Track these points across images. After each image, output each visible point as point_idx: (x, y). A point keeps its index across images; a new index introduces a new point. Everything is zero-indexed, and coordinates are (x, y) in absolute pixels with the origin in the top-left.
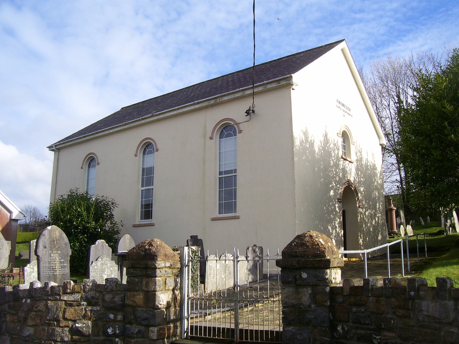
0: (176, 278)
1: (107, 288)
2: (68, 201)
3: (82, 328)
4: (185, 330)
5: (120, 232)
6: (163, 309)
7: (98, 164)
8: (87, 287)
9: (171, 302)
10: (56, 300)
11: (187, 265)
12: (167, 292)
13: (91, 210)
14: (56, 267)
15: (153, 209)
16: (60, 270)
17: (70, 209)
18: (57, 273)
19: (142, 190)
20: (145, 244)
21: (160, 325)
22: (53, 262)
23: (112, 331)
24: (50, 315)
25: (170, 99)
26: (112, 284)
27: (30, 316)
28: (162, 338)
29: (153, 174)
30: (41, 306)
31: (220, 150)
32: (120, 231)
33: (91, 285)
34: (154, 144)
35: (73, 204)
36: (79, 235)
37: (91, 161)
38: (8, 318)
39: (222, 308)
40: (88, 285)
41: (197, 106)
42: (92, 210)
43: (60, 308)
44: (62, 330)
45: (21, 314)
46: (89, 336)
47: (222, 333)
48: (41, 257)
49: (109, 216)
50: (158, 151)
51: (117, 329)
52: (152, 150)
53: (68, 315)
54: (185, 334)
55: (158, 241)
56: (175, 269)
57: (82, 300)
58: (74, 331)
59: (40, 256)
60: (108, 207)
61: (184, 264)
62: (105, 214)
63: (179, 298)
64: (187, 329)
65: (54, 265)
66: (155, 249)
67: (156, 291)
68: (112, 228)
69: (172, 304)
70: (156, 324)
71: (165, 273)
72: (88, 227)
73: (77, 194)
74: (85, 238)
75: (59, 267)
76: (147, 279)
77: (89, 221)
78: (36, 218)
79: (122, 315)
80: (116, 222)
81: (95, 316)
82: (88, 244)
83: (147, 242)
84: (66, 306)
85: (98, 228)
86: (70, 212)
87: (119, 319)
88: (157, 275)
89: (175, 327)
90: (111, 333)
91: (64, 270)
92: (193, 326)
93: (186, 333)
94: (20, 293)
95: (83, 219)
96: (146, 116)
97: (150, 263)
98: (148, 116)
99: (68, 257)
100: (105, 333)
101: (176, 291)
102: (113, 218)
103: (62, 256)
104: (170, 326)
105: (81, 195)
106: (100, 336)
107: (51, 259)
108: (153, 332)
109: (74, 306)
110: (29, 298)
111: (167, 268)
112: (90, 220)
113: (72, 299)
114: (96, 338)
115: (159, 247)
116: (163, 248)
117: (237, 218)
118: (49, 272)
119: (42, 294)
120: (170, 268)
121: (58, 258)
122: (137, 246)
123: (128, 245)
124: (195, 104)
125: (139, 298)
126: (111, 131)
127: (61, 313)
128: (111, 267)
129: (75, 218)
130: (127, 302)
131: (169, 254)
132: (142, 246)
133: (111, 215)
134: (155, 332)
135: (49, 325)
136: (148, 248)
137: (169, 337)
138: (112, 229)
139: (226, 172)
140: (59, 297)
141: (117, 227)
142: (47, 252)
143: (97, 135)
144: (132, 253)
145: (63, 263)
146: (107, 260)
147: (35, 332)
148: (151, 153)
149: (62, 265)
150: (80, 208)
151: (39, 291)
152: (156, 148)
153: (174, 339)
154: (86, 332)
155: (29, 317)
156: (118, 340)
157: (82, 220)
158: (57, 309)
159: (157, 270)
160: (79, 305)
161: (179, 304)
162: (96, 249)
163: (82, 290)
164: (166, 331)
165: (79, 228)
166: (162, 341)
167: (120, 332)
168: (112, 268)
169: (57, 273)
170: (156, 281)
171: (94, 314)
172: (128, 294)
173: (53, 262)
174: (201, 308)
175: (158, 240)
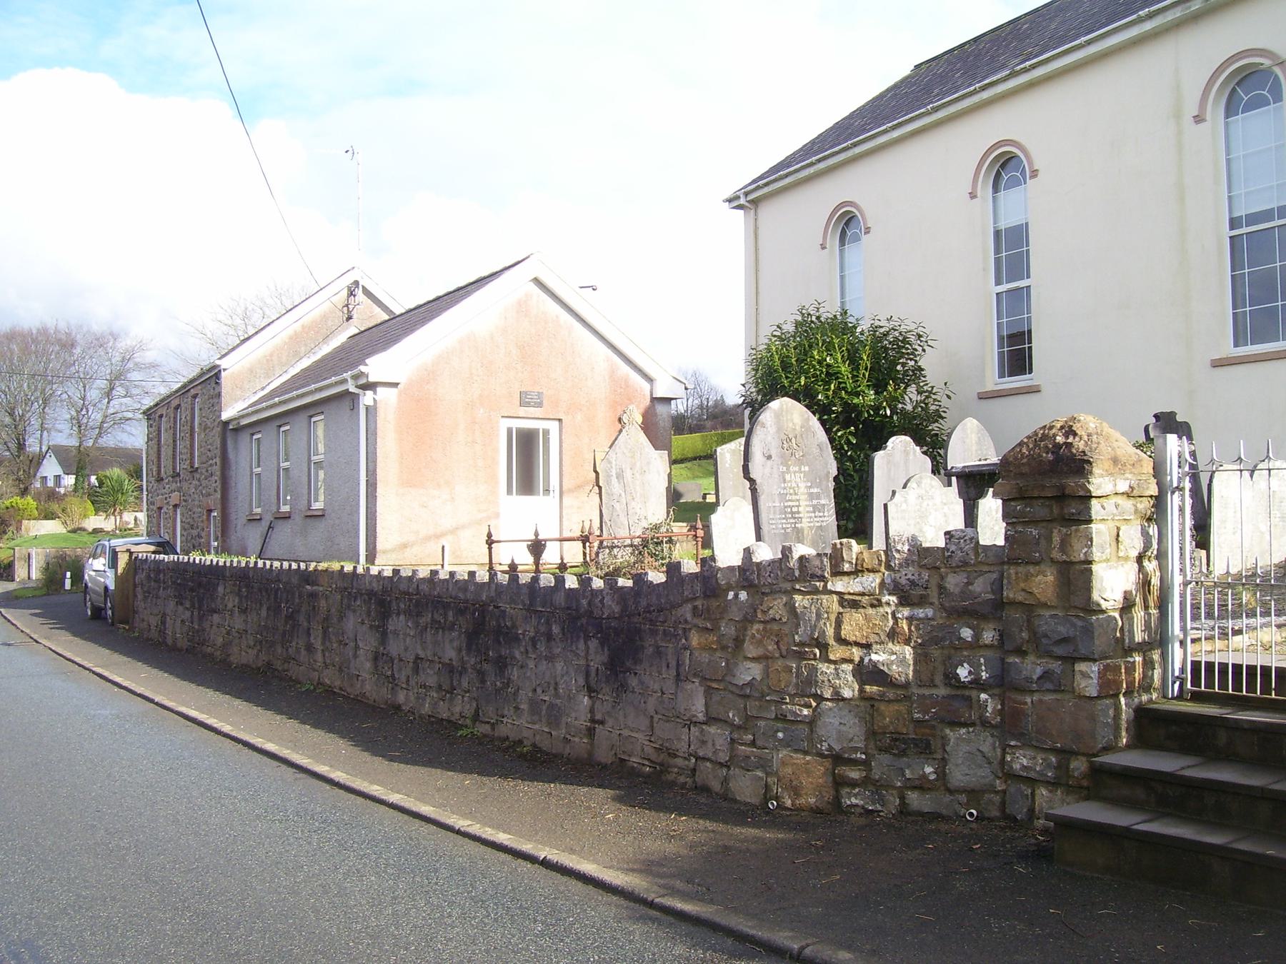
0: (1146, 524)
1: (950, 556)
2: (798, 339)
3: (887, 665)
4: (1177, 673)
5: (943, 414)
6: (1112, 614)
7: (868, 230)
8: (897, 556)
9: (1134, 592)
10: (816, 591)
11: (1177, 488)
12: (1122, 565)
13: (862, 359)
14: (801, 509)
15: (1033, 345)
16: (811, 517)
17: (804, 360)
18: (803, 525)
19: (997, 294)
20: (1054, 431)
21: (1106, 658)
22: (791, 494)
23: (970, 672)
24: (801, 631)
25: (1058, 20)
26: (963, 545)
27: (749, 633)
28: (1111, 693)
29: (1027, 245)
30: (777, 607)
31: (1228, 153)
32: (945, 412)
33: (906, 551)
34: (860, 217)
35: (811, 346)
36: (834, 429)
37: (847, 224)
38: (695, 639)
39: (1275, 615)
40: (898, 551)
41: (1148, 26)
42: (865, 358)
43: (827, 613)
44: (836, 669)
45: (727, 630)
46: (906, 685)
47: (1275, 689)
48: (761, 483)
49: (911, 373)
50: (1037, 175)
51: (983, 668)
52: (1018, 174)
53: (846, 631)
54: (1177, 686)
55: (1088, 423)
56: (1141, 499)
57: (885, 592)
58: (868, 673)
59: (758, 481)
60: (908, 349)
61: (1169, 483)
62: (899, 368)
63: (1155, 581)
64: (1183, 670)
65: (794, 504)
66: (1082, 442)
67: (1090, 562)
68: (923, 405)
69: (1138, 599)
70: (1094, 654)
71: (1115, 511)
72: (856, 406)
73: (818, 318)
74: (850, 437)
75: (808, 509)
76: (1064, 530)
77: (859, 389)
78: (700, 397)
79: (995, 629)
80: (933, 387)
81: (921, 632)
82: (860, 451)
83: (1058, 426)
84: (843, 607)
85: (885, 408)
86: (806, 367)
87: (986, 642)
88: (1093, 518)
89: (1149, 664)
90: (966, 680)
91: (820, 517)
92: (1200, 662)
93: (1178, 683)
94: (719, 575)
95: (843, 385)
96: (995, 78)
97: (1071, 482)
98: (999, 76)
99: (828, 481)
100: (951, 679)
101: (1146, 563)
102: (924, 377)
103: (813, 479)
104: (1134, 662)
105: (831, 319)
106: (935, 686)
107: (785, 488)
108: (1085, 675)
109: (864, 607)
110: (743, 588)
111: (1120, 496)
112: (860, 386)
113: (858, 589)
114: (926, 692)
115: (1095, 436)
116: (1107, 439)
118: (784, 521)
119: (777, 577)
120: (1128, 496)
121: (802, 485)
122: (1030, 437)
123: (974, 448)
124: (1141, 20)
125: (1044, 582)
126: (896, 134)
127: (831, 625)
128: (945, 504)
129: (820, 383)
130: (1008, 594)
131: (1124, 456)
132: (1045, 436)
133: (916, 369)
134: (1092, 675)
135: (801, 656)
136: (1064, 440)
137: (1132, 692)
138: (922, 407)
139: (1253, 219)
140: (822, 584)
141: (935, 400)
142: (775, 470)
143: (857, 150)
144: (1016, 459)
145: (818, 496)
146: (932, 487)
147: (766, 673)
148: (1015, 183)
149: (815, 502)
150: (831, 355)
151: (769, 569)
152: (1030, 168)
153: (1145, 698)
154: (900, 676)
155: (748, 638)
156: (987, 697)
157: (839, 389)
158: (819, 616)
159: (1094, 502)
160: (877, 604)
161: (1156, 598)
162: (889, 462)
163: (883, 565)
164: (1123, 674)
165: (834, 408)
166: (1112, 701)
167: (990, 677)
168: (946, 507)
169: (803, 525)
170: (1091, 533)
171: (918, 629)
172: (1011, 571)
173: (791, 494)
174: (1209, 615)
175: (1090, 418)
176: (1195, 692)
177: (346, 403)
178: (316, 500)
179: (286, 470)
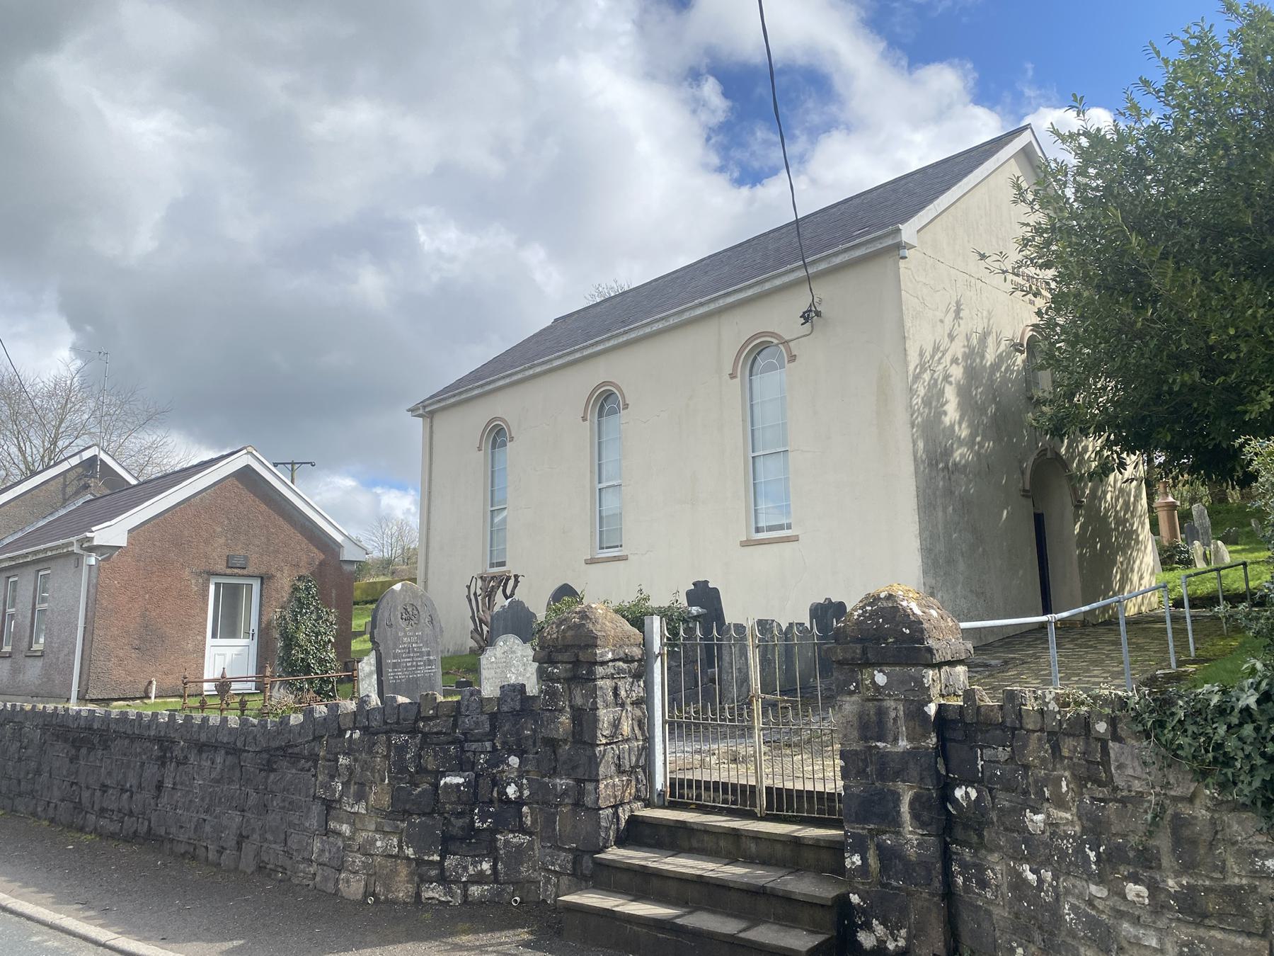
34: (617, 393)
117: (795, 539)
148: (614, 412)
176: (671, 801)
177: (72, 560)
178: (37, 642)
179: (12, 616)
